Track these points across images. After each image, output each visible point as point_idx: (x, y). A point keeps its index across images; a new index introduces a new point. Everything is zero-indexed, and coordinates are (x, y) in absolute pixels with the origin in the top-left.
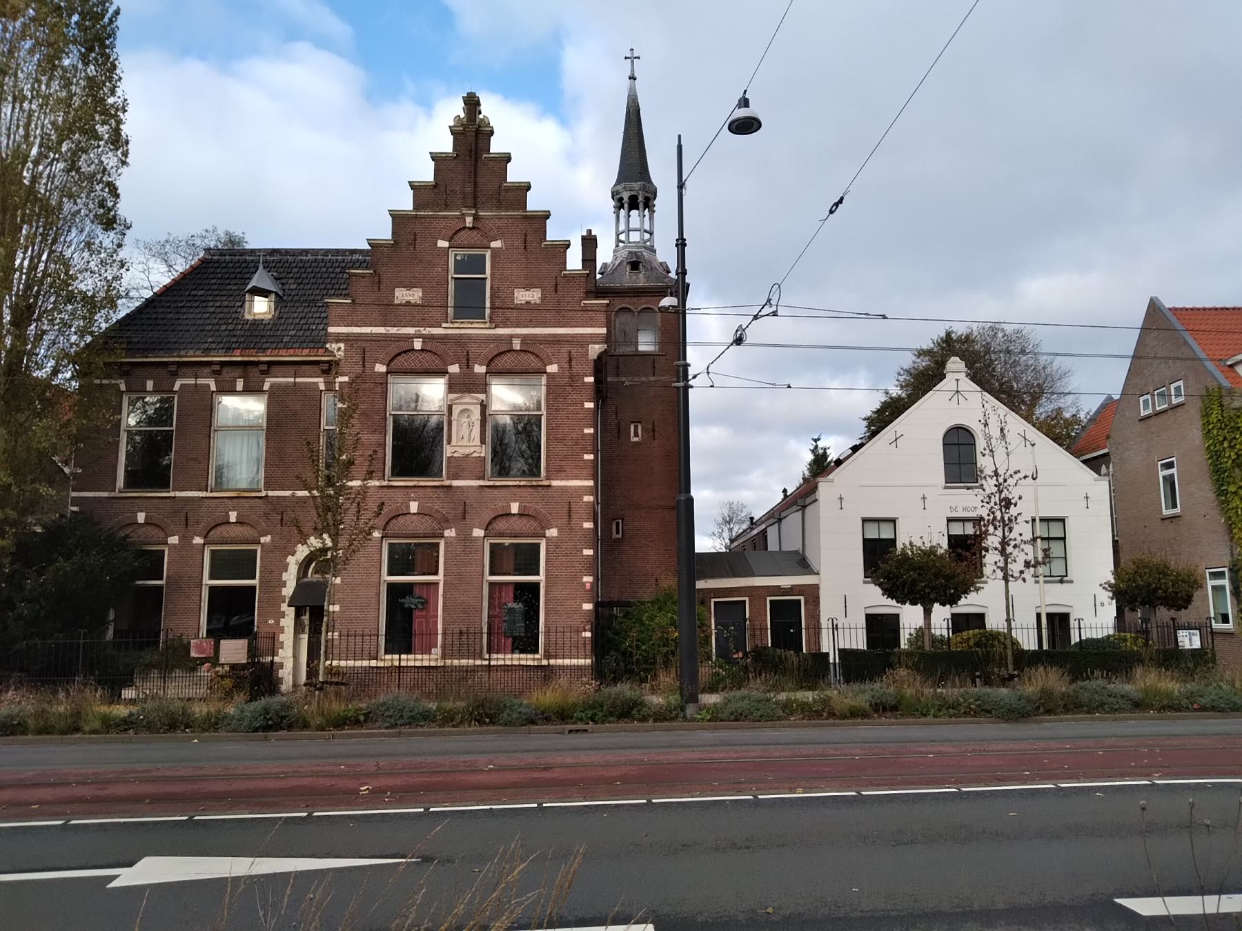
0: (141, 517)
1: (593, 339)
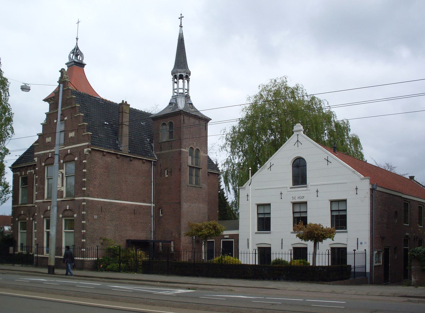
0: (22, 212)
1: (84, 147)
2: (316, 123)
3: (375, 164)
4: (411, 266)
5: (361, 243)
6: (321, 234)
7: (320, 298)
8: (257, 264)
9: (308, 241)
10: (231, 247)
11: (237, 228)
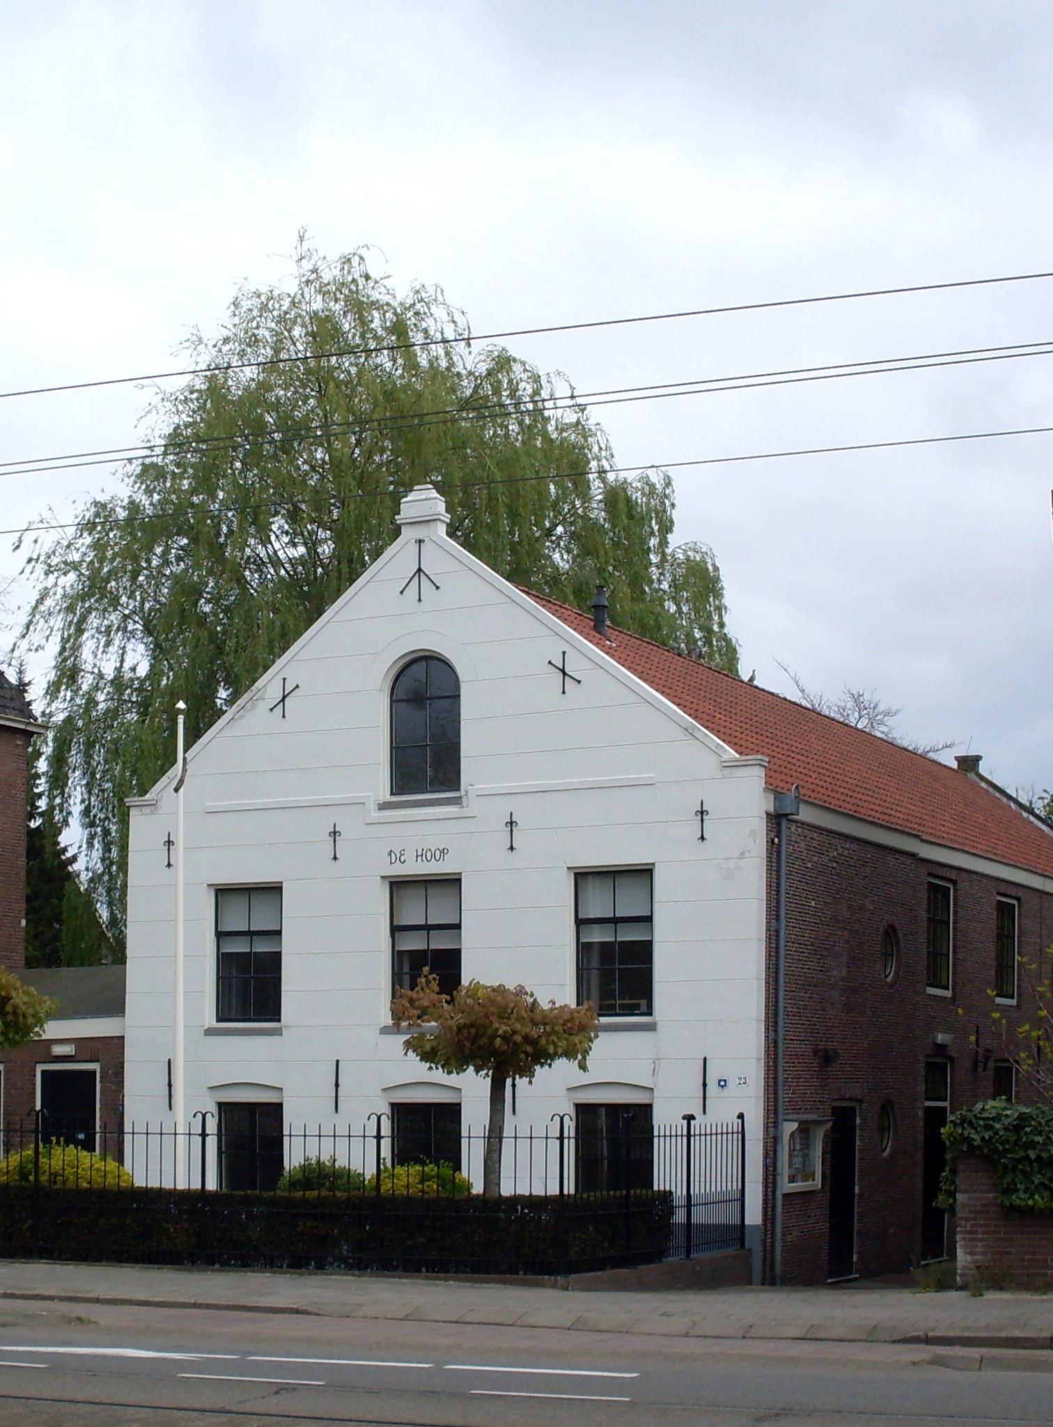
2: (511, 481)
3: (793, 695)
4: (952, 1194)
5: (723, 1084)
6: (527, 1039)
7: (515, 1357)
8: (212, 1185)
9: (461, 1069)
10: (80, 1101)
11: (116, 1006)
